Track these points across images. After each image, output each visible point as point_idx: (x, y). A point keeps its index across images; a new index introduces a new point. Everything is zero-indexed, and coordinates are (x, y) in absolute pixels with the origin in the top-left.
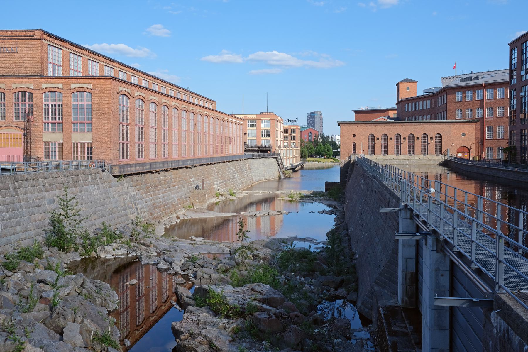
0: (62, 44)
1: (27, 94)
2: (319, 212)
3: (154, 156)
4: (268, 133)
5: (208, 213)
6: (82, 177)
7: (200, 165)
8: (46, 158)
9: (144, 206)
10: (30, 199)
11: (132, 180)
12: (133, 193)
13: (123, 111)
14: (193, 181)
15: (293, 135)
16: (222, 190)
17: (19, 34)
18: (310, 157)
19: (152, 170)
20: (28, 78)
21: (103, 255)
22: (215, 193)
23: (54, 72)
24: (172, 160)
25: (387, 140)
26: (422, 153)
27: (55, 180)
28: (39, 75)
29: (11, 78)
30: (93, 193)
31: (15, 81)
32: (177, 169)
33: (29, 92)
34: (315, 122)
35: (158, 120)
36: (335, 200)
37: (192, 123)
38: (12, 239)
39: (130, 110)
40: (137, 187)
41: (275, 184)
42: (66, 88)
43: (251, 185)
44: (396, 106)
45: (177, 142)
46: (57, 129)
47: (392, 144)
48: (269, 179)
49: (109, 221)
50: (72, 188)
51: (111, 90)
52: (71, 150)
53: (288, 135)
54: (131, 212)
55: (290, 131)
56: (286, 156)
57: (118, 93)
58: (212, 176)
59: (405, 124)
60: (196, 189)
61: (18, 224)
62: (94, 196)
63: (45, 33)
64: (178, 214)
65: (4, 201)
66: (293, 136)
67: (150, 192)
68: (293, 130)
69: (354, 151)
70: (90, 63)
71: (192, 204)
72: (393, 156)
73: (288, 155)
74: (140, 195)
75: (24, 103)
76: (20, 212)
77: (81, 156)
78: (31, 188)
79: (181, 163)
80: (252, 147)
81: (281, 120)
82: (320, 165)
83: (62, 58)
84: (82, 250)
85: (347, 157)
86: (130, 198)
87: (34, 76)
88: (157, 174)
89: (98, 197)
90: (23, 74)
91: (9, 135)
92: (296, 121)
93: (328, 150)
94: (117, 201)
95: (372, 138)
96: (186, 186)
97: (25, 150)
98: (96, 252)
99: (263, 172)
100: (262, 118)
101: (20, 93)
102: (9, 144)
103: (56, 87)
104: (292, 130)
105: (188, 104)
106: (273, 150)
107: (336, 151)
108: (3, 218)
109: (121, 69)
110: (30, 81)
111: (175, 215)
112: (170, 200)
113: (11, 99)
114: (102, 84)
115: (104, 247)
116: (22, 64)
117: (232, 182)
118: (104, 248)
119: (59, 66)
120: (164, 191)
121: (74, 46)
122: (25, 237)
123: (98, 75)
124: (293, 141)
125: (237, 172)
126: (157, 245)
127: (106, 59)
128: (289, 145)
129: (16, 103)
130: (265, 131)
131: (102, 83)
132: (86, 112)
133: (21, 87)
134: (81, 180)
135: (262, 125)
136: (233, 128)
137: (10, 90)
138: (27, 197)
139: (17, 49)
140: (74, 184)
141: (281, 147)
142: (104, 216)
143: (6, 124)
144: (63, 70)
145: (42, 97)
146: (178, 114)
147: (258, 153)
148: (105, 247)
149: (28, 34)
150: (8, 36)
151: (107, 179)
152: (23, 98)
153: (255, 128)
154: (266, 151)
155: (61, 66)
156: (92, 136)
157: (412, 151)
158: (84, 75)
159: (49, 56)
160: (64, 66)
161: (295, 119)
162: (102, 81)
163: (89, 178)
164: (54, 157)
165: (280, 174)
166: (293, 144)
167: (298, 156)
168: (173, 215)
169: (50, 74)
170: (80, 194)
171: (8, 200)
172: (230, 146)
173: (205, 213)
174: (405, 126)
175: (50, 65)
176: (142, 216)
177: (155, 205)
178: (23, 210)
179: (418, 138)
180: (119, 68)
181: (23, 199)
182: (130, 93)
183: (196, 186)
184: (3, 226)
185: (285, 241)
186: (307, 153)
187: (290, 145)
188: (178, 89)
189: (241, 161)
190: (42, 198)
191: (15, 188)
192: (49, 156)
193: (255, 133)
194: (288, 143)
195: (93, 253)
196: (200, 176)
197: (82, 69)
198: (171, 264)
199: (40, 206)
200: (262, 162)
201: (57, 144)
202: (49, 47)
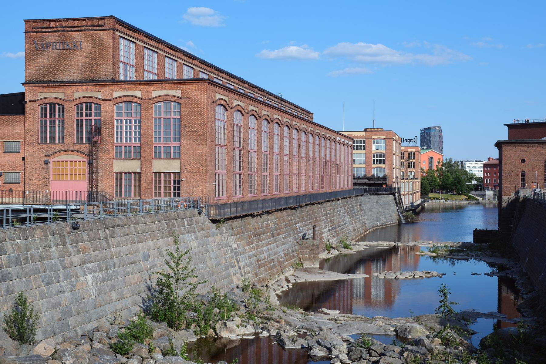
2: (486, 274)
4: (382, 159)
5: (327, 275)
8: (117, 195)
13: (220, 128)
15: (411, 160)
16: (333, 240)
17: (83, 23)
18: (432, 192)
20: (95, 84)
21: (225, 334)
22: (325, 245)
23: (125, 75)
27: (148, 227)
28: (109, 79)
29: (73, 84)
31: (77, 89)
33: (95, 104)
38: (107, 310)
40: (238, 236)
41: (393, 233)
42: (145, 97)
43: (364, 233)
48: (386, 225)
50: (167, 237)
51: (207, 99)
52: (152, 183)
53: (404, 160)
56: (404, 192)
58: (320, 220)
60: (303, 239)
65: (96, 256)
66: (411, 162)
67: (252, 244)
68: (411, 154)
70: (167, 61)
74: (242, 248)
75: (88, 118)
82: (448, 203)
83: (136, 55)
84: (196, 326)
85: (512, 193)
86: (231, 252)
88: (259, 218)
91: (69, 163)
93: (458, 183)
94: (217, 257)
96: (292, 235)
97: (89, 185)
99: (378, 215)
100: (373, 137)
101: (48, 106)
102: (69, 175)
104: (409, 154)
105: (291, 117)
106: (389, 183)
107: (470, 183)
110: (97, 88)
111: (283, 277)
112: (275, 255)
113: (71, 114)
114: (196, 91)
116: (87, 65)
117: (343, 228)
118: (225, 325)
121: (149, 39)
123: (176, 78)
124: (411, 170)
126: (291, 321)
128: (405, 175)
129: (78, 118)
130: (377, 155)
131: (195, 89)
132: (172, 130)
133: (86, 97)
134: (176, 226)
135: (373, 147)
137: (71, 101)
138: (120, 251)
139: (80, 45)
143: (65, 148)
144: (136, 71)
145: (113, 110)
149: (95, 22)
152: (88, 112)
154: (381, 185)
155: (134, 66)
158: (160, 79)
160: (138, 66)
161: (414, 138)
162: (195, 87)
164: (128, 193)
165: (400, 217)
166: (411, 174)
167: (418, 192)
169: (122, 78)
171: (100, 254)
173: (324, 273)
175: (122, 66)
178: (117, 268)
181: (116, 253)
183: (304, 235)
184: (97, 291)
186: (428, 187)
187: (407, 175)
188: (267, 96)
189: (351, 199)
190: (136, 252)
191: (106, 238)
192: (121, 192)
193: (363, 158)
195: (211, 332)
197: (158, 70)
198: (330, 350)
199: (135, 263)
200: (375, 200)
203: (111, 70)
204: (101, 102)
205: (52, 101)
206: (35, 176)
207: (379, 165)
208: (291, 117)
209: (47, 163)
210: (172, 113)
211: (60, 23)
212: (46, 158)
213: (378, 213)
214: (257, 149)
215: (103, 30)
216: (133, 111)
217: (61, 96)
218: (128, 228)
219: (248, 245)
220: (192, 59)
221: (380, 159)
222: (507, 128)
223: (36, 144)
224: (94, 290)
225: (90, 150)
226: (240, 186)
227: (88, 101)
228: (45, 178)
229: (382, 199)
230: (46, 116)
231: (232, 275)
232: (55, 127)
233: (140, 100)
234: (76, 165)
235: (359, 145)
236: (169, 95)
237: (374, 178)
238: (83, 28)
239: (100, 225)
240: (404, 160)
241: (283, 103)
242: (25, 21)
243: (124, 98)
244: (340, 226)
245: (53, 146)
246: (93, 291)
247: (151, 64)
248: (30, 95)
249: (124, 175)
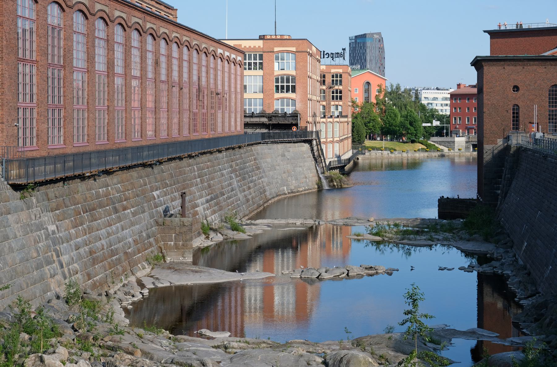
9: (75, 258)
15: (336, 87)
16: (213, 217)
22: (200, 226)
24: (114, 147)
34: (368, 58)
36: (487, 240)
40: (57, 212)
43: (263, 205)
55: (329, 80)
56: (333, 137)
58: (192, 185)
64: (139, 274)
66: (337, 90)
67: (82, 224)
69: (516, 127)
71: (161, 252)
73: (330, 135)
85: (499, 140)
86: (46, 239)
88: (91, 181)
93: (411, 124)
94: (23, 247)
96: (146, 209)
99: (285, 176)
100: (276, 49)
104: (333, 77)
106: (302, 124)
107: (429, 125)
111: (133, 279)
117: (230, 198)
124: (337, 103)
125: (237, 176)
126: (152, 352)
128: (327, 110)
130: (282, 79)
135: (276, 65)
148: (45, 357)
153: (260, 72)
154: (289, 126)
161: (340, 51)
167: (347, 138)
173: (201, 272)
177: (94, 255)
185: (435, 338)
187: (329, 111)
189: (242, 151)
193: (259, 83)
194: (324, 106)
196: (171, 185)
200: (280, 152)
207: (285, 95)
213: (284, 173)
222: (488, 36)
229: (291, 150)
231: (49, 276)
237: (278, 116)
244: (224, 195)
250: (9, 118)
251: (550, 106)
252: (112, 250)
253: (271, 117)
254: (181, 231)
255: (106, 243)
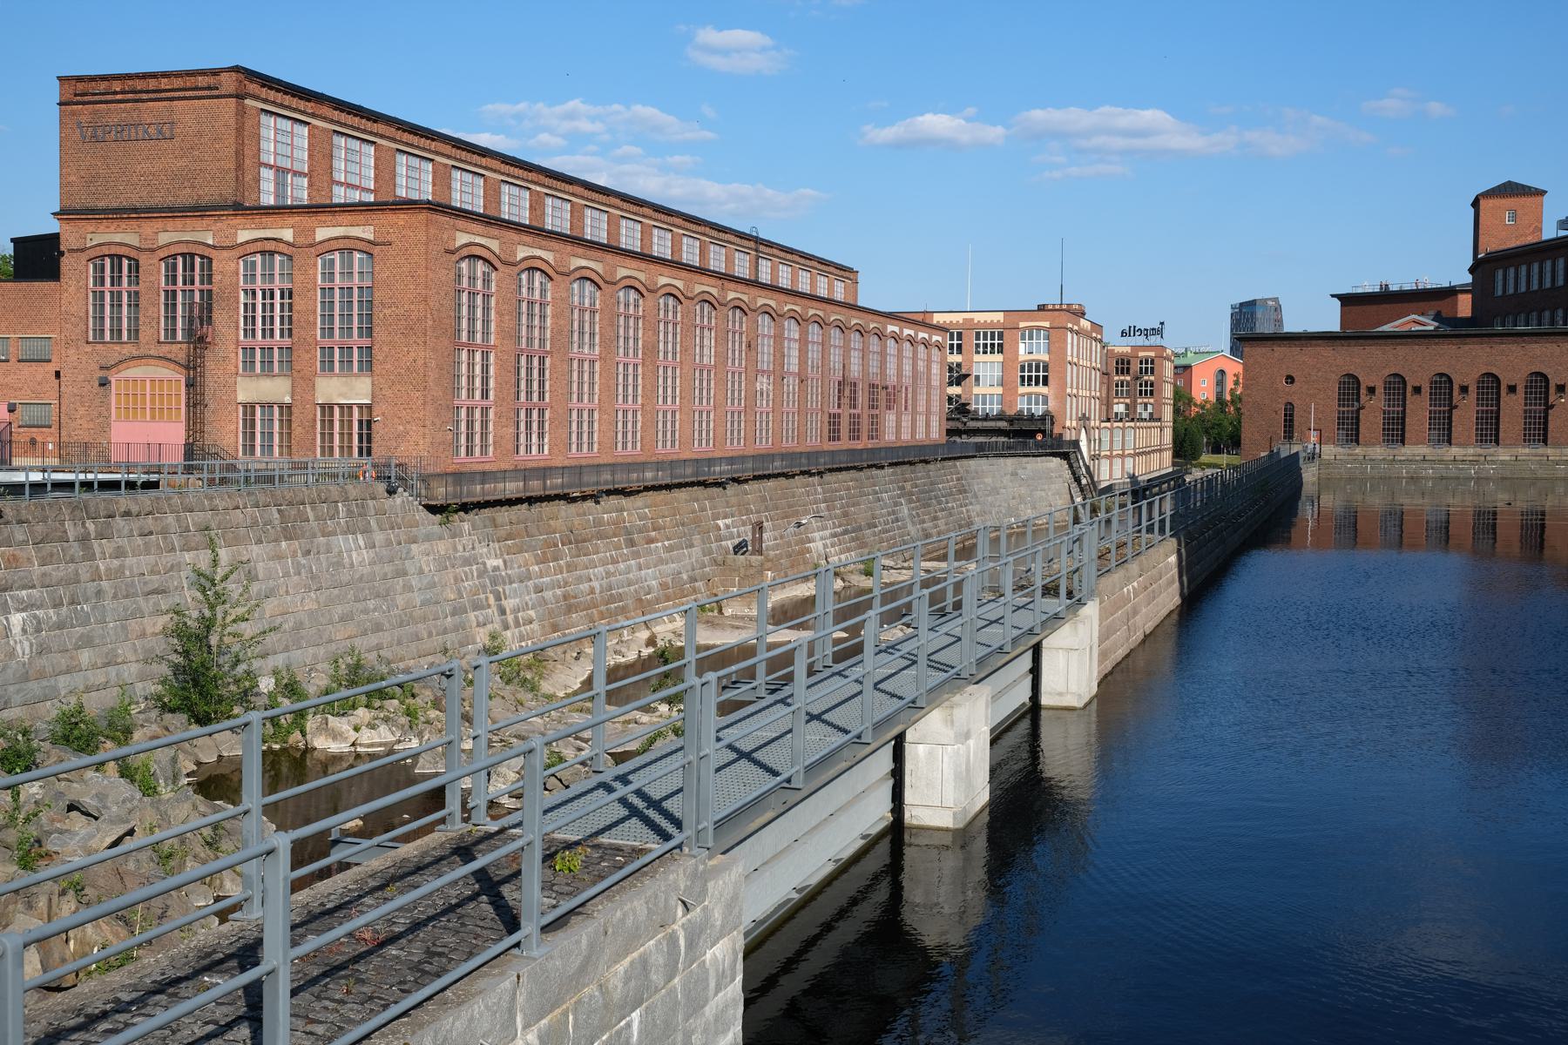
0: (310, 107)
1: (198, 260)
3: (735, 441)
6: (313, 509)
7: (756, 478)
8: (245, 453)
9: (530, 603)
10: (131, 570)
11: (494, 520)
12: (492, 562)
14: (727, 527)
15: (1146, 378)
17: (178, 83)
19: (566, 491)
20: (199, 214)
21: (321, 743)
25: (1404, 394)
26: (1528, 439)
29: (155, 215)
30: (350, 557)
32: (668, 487)
33: (202, 257)
35: (601, 335)
37: (855, 341)
38: (61, 685)
39: (497, 303)
42: (302, 241)
44: (1468, 279)
45: (740, 404)
46: (276, 364)
47: (1419, 411)
49: (399, 643)
52: (314, 427)
53: (1128, 378)
54: (481, 619)
56: (1111, 450)
57: (452, 253)
59: (1468, 340)
60: (736, 553)
61: (87, 642)
62: (352, 565)
63: (252, 75)
64: (658, 629)
65: (44, 575)
66: (1146, 383)
68: (1147, 363)
72: (1423, 450)
74: (520, 567)
75: (188, 287)
76: (93, 609)
77: (342, 448)
78: (139, 541)
79: (689, 471)
80: (986, 418)
81: (1093, 330)
83: (309, 150)
86: (479, 577)
87: (215, 208)
88: (590, 504)
89: (367, 570)
90: (190, 202)
92: (1158, 332)
94: (432, 585)
95: (1350, 388)
97: (189, 430)
98: (304, 734)
100: (1022, 325)
101: (180, 260)
102: (148, 409)
103: (274, 239)
104: (1141, 363)
108: (39, 623)
109: (508, 175)
110: (206, 222)
112: (629, 585)
113: (152, 279)
114: (404, 227)
115: (327, 719)
119: (296, 173)
120: (611, 556)
122: (103, 680)
124: (1146, 400)
125: (910, 501)
127: (459, 148)
130: (1030, 366)
132: (356, 311)
134: (311, 517)
135: (1022, 347)
136: (915, 358)
137: (153, 250)
138: (122, 567)
139: (171, 130)
140: (284, 529)
141: (1089, 419)
142: (382, 630)
143: (142, 352)
144: (311, 185)
145: (238, 269)
146: (679, 315)
147: (1006, 439)
149: (202, 81)
150: (148, 92)
151: (403, 518)
153: (999, 357)
154: (1032, 434)
155: (305, 175)
156: (373, 385)
157: (1444, 431)
159: (264, 145)
160: (315, 174)
161: (1157, 326)
163: (338, 513)
166: (1146, 409)
168: (637, 634)
169: (268, 199)
170: (303, 561)
171: (57, 571)
172: (890, 418)
173: (745, 628)
174: (1466, 348)
175: (267, 174)
176: (520, 632)
179: (1512, 389)
180: (503, 174)
181: (108, 569)
182: (497, 252)
183: (740, 543)
189: (931, 467)
191: (84, 539)
193: (997, 373)
197: (376, 182)
200: (1010, 469)
201: (276, 409)
202: (264, 118)
203: (233, 184)
204: (213, 254)
205: (114, 250)
206: (82, 411)
207: (1033, 389)
208: (720, 282)
209: (104, 383)
210: (356, 276)
211: (130, 83)
212: (102, 373)
213: (1013, 498)
214: (600, 354)
215: (217, 97)
216: (277, 271)
217: (132, 239)
218: (156, 519)
219: (542, 561)
220: (479, 155)
221: (1038, 374)
222: (1337, 303)
223: (82, 343)
224: (26, 644)
225: (189, 356)
226: (541, 436)
227: (186, 251)
228: (100, 414)
229: (1029, 466)
230: (103, 284)
231: (475, 624)
232: (120, 306)
233: (291, 248)
234: (161, 389)
235: (989, 342)
236: (348, 238)
237: (1022, 419)
238: (177, 94)
239: (69, 511)
240: (1128, 378)
241: (762, 248)
242: (59, 78)
243: (259, 244)
244: (876, 527)
245: (117, 348)
246: (22, 646)
247: (354, 168)
248: (71, 236)
249: (258, 410)
250: (436, 420)
251: (1339, 406)
252: (611, 595)
253: (1012, 421)
254: (748, 573)
255: (601, 585)
